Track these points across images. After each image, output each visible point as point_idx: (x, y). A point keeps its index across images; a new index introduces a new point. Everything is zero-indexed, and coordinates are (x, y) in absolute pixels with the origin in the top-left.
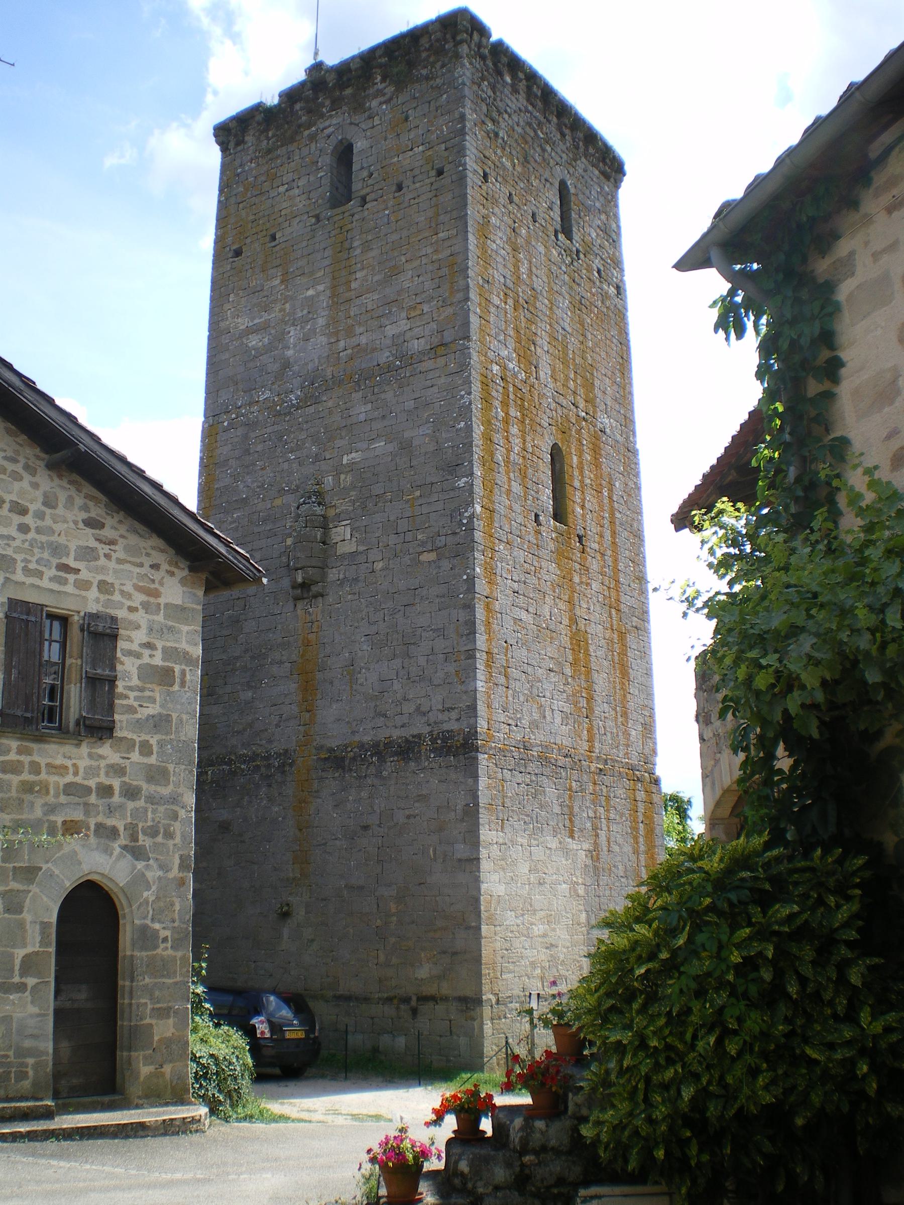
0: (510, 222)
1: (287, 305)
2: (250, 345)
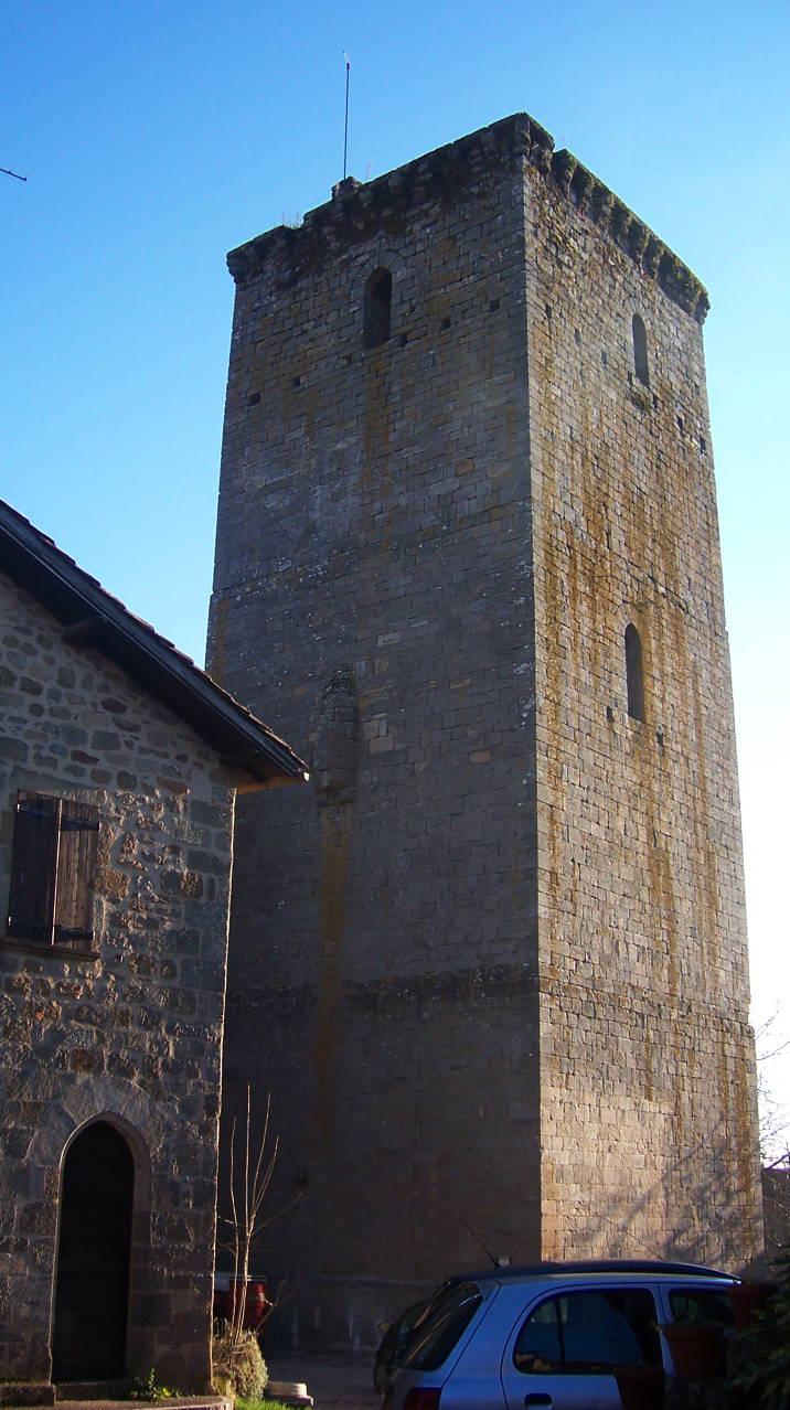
0: (577, 364)
1: (313, 460)
2: (268, 506)
